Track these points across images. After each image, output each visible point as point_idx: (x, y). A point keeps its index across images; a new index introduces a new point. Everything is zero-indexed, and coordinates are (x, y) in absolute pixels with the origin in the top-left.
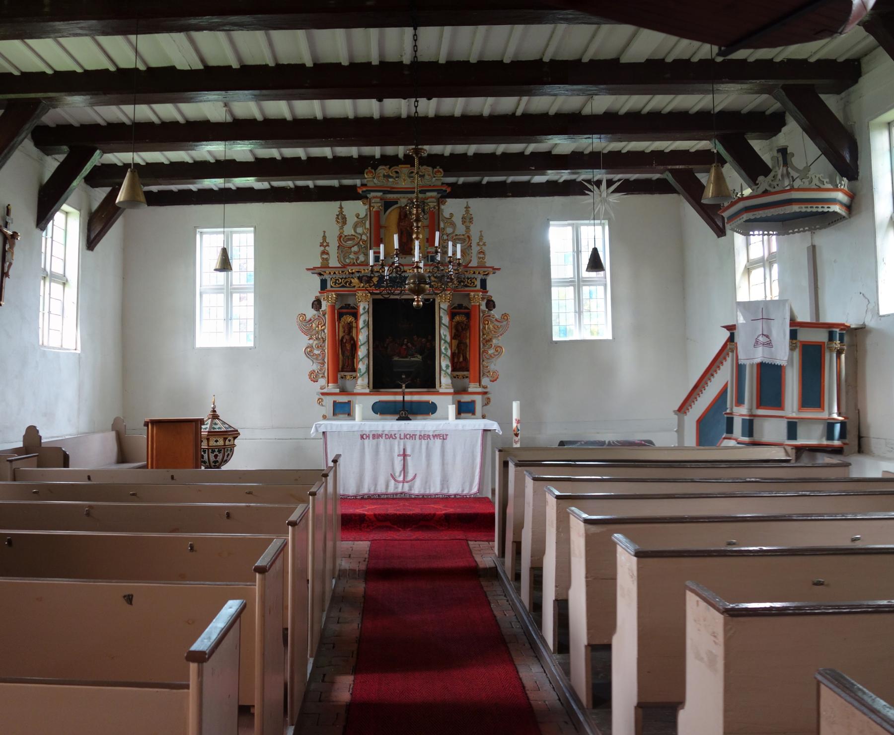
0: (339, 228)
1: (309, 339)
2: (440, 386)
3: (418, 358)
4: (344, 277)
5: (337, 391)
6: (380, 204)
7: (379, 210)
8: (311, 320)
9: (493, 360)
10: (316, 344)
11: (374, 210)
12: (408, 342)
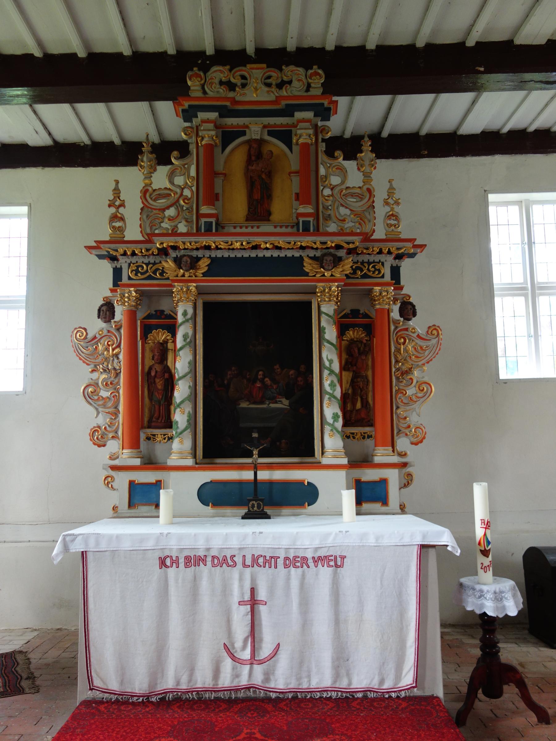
0: (143, 177)
1: (93, 371)
2: (323, 453)
3: (284, 404)
4: (152, 261)
5: (137, 462)
6: (213, 133)
7: (212, 143)
8: (95, 337)
9: (416, 406)
10: (104, 380)
11: (203, 143)
12: (265, 377)
